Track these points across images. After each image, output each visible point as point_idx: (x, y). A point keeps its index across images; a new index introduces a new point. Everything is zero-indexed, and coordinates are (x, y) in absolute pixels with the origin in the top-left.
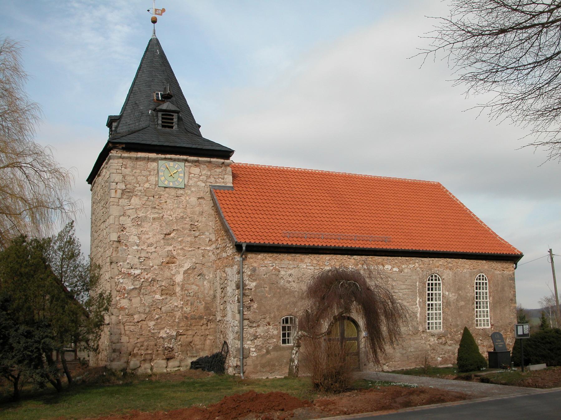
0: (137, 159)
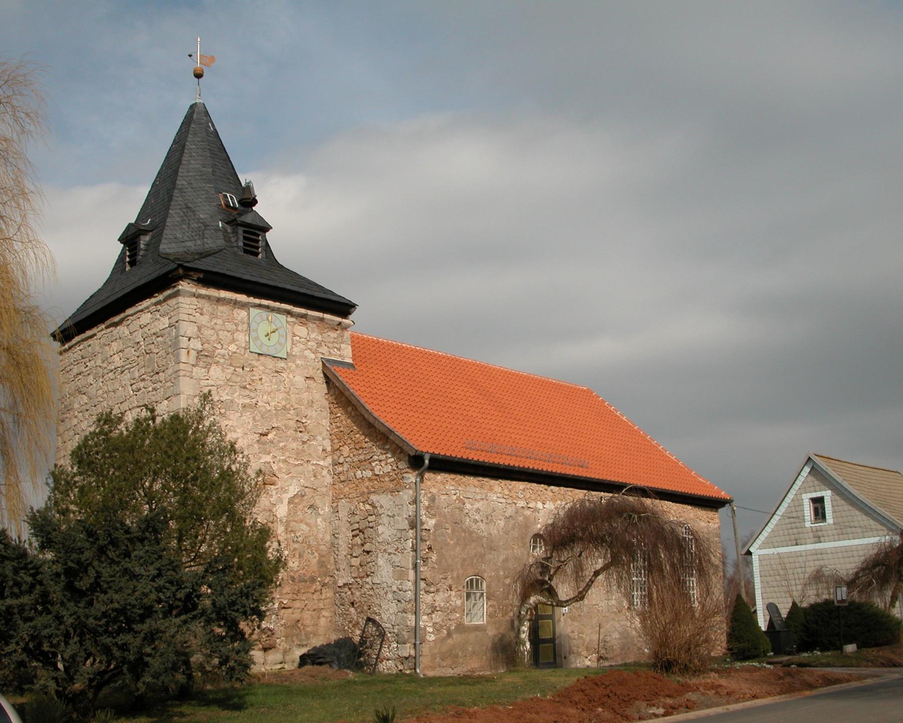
0: (219, 300)
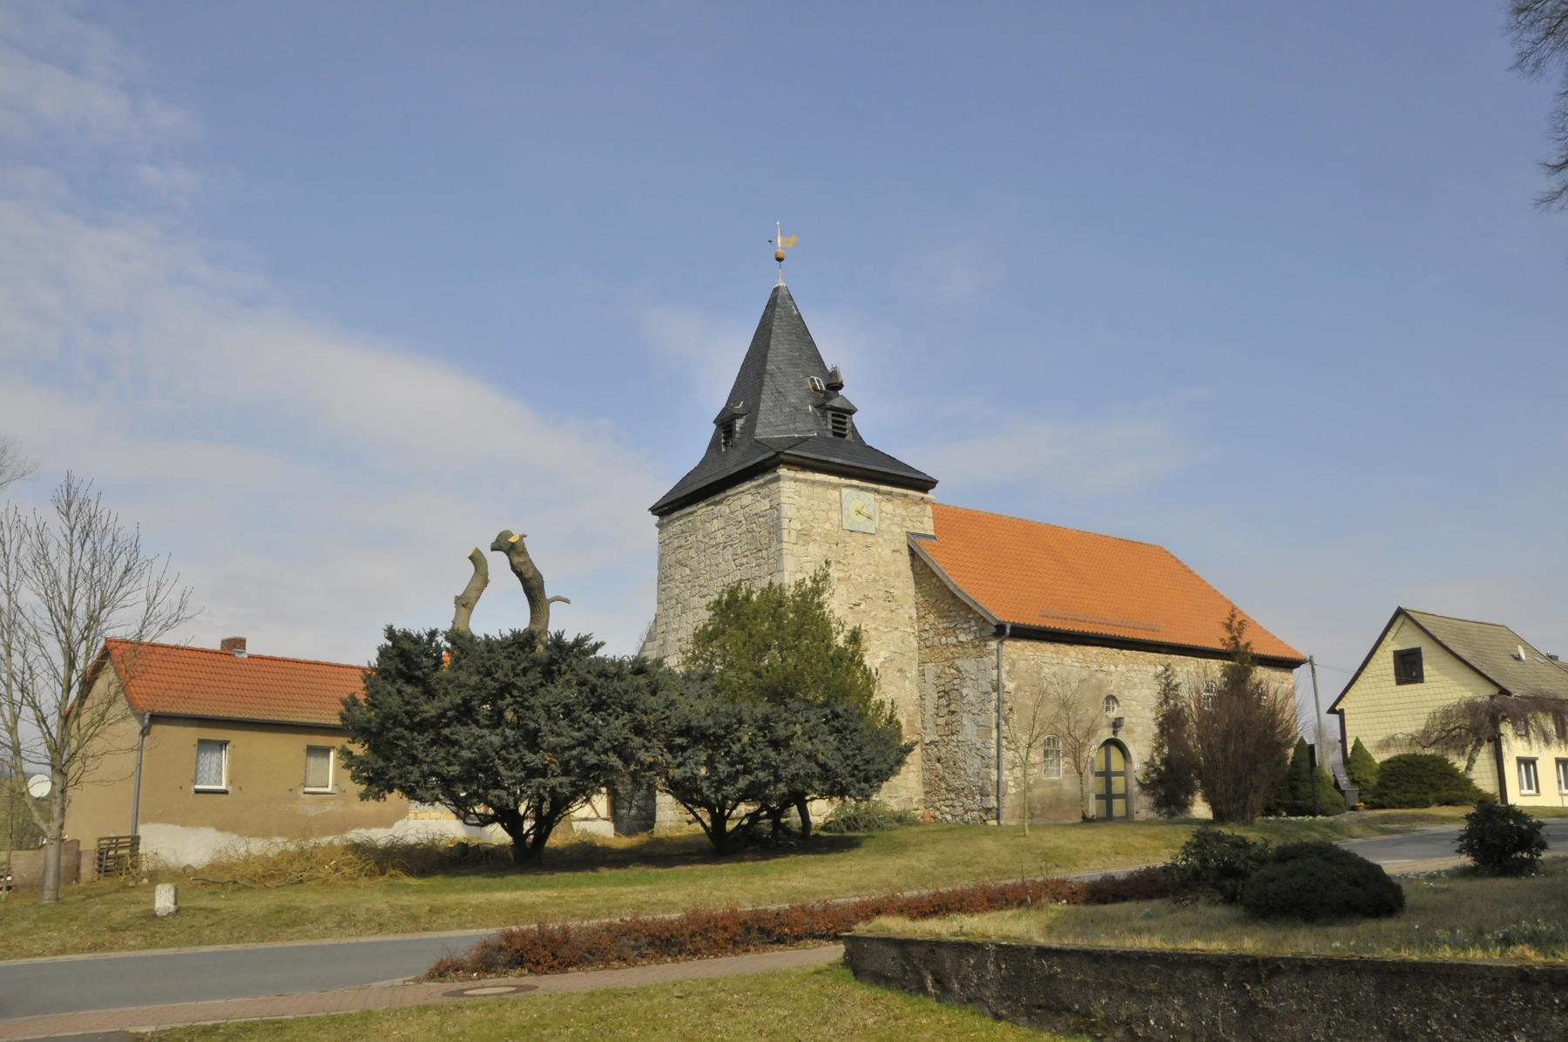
0: (814, 482)
